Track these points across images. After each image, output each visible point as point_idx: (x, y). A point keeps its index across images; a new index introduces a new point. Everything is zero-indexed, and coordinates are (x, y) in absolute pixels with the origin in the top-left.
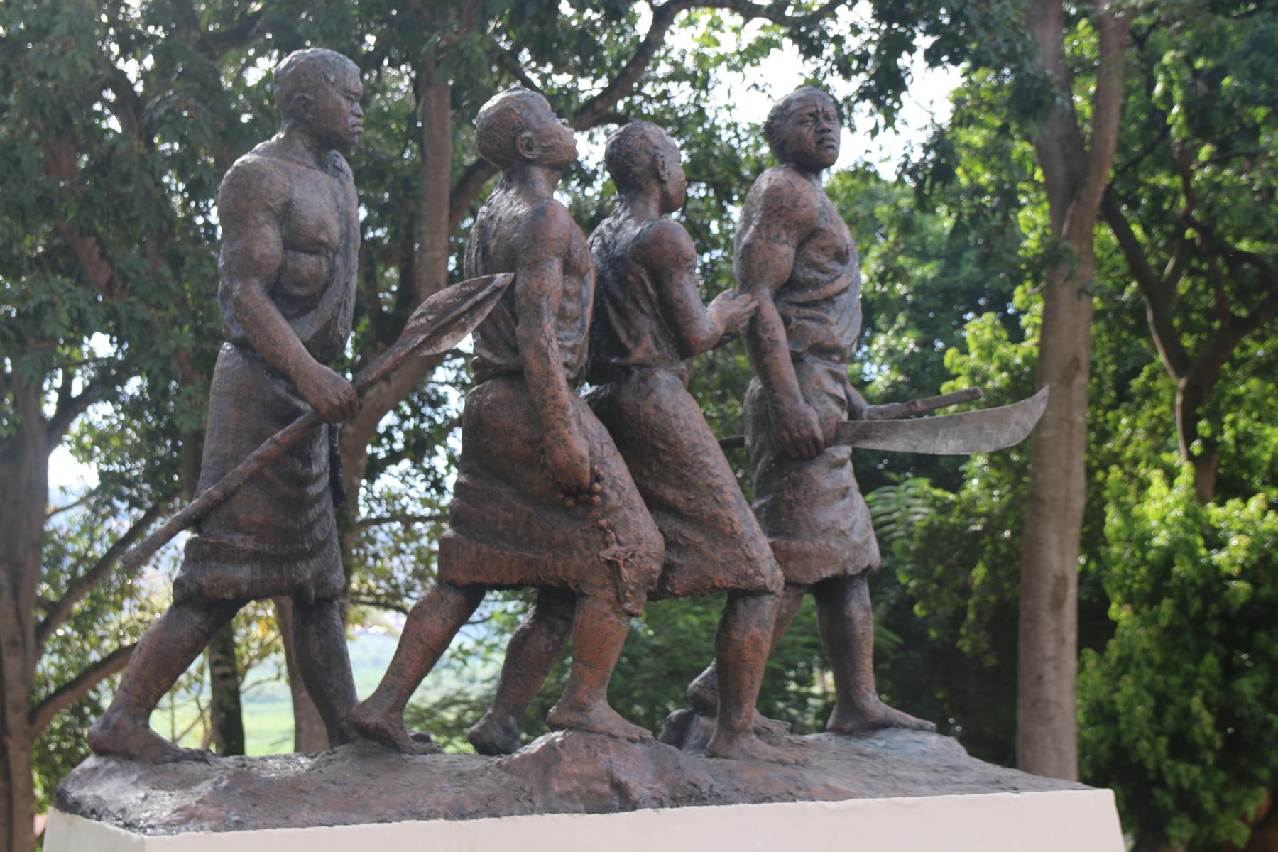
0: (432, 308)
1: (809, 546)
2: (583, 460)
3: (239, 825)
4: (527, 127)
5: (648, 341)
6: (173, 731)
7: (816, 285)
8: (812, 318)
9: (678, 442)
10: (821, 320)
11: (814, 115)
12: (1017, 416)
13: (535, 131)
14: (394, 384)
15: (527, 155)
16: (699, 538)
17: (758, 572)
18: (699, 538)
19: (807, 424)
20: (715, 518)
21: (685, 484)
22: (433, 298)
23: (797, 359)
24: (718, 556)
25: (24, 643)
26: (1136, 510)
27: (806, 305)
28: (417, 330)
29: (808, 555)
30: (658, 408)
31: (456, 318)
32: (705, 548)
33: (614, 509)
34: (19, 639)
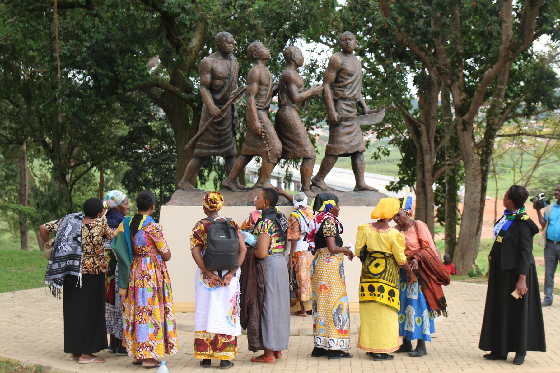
0: (234, 93)
1: (336, 146)
2: (258, 128)
3: (182, 205)
4: (255, 51)
5: (285, 99)
6: (514, 180)
7: (342, 82)
8: (340, 90)
9: (289, 123)
10: (342, 91)
11: (346, 39)
12: (379, 115)
13: (257, 52)
14: (494, 69)
15: (255, 57)
16: (294, 145)
17: (307, 153)
18: (294, 145)
19: (333, 117)
20: (298, 141)
21: (291, 133)
22: (234, 91)
23: (335, 101)
24: (298, 149)
25: (431, 150)
26: (524, 132)
27: (341, 87)
28: (231, 98)
29: (336, 149)
30: (285, 115)
31: (238, 96)
32: (296, 148)
33: (269, 139)
34: (429, 148)
